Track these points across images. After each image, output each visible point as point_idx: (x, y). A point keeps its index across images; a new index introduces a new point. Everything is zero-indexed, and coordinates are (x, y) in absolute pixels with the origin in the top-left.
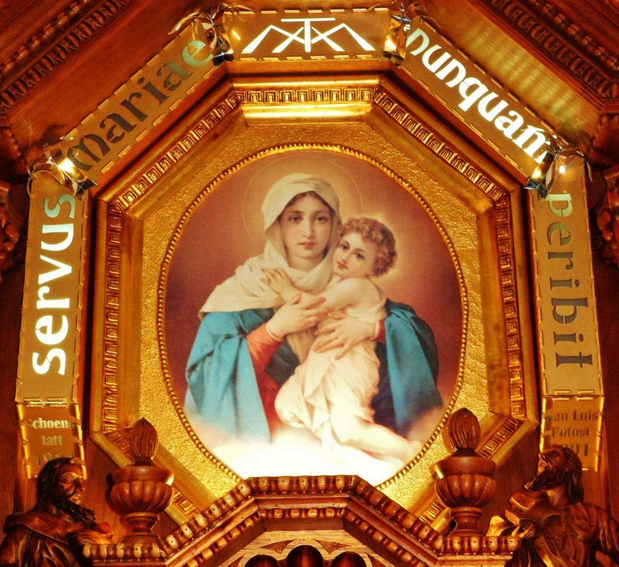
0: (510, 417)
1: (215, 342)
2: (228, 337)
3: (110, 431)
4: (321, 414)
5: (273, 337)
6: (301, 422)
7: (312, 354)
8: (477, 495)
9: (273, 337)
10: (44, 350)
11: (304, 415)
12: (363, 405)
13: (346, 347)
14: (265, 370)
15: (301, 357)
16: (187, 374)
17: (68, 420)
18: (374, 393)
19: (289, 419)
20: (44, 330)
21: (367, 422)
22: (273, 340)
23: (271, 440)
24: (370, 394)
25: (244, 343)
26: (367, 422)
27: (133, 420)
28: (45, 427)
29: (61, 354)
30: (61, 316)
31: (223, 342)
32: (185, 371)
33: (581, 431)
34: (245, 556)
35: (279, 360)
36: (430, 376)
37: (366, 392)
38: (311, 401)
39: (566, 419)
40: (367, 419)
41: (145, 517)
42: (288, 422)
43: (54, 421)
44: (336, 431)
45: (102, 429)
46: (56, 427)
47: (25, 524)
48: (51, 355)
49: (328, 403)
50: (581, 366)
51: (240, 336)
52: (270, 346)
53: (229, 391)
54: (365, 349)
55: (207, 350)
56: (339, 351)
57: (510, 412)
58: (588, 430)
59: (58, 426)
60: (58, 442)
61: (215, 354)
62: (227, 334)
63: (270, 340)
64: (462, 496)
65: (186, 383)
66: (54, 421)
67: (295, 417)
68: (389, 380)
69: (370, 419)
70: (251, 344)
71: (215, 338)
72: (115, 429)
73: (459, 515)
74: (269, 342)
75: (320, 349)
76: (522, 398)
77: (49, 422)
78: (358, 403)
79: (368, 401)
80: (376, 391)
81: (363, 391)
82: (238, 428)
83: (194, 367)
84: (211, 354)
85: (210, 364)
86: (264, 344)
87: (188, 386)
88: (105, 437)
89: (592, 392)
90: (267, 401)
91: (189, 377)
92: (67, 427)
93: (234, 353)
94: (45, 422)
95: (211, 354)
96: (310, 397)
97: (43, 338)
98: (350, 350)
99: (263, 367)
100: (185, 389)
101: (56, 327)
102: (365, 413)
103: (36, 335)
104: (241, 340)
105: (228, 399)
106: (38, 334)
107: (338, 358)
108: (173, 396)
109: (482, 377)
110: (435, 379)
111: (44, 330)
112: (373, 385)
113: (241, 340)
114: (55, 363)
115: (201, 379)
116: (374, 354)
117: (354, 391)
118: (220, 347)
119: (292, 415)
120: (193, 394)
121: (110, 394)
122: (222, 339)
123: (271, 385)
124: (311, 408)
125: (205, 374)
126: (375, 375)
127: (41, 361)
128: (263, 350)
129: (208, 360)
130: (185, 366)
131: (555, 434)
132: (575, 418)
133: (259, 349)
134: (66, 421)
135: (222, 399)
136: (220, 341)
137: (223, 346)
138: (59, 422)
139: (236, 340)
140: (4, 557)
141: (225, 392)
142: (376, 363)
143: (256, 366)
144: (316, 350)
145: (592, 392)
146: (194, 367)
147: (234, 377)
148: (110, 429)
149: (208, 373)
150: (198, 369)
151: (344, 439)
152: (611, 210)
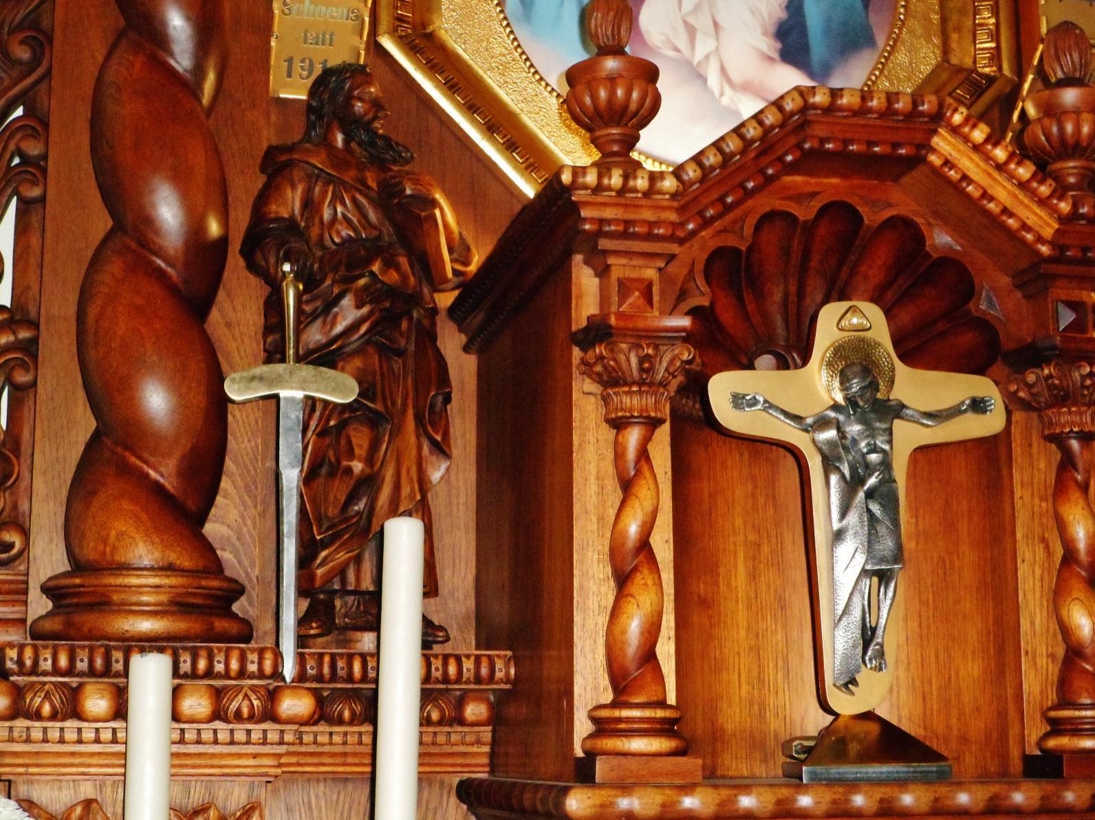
0: (974, 70)
4: (704, 46)
6: (677, 50)
8: (1084, 144)
11: (682, 43)
12: (765, 33)
18: (780, 18)
19: (660, 44)
24: (775, 19)
26: (771, 59)
27: (304, 571)
34: (822, 194)
37: (770, 15)
38: (692, 20)
41: (618, 134)
42: (658, 47)
44: (727, 66)
47: (644, 553)
49: (716, 24)
50: (1091, 5)
57: (975, 62)
64: (1077, 145)
67: (668, 41)
69: (776, 56)
76: (993, 45)
78: (759, 30)
79: (772, 29)
80: (783, 15)
81: (765, 14)
88: (399, 40)
96: (687, 14)
102: (770, 46)
109: (933, 11)
112: (780, 6)
117: (752, 12)
119: (663, 38)
124: (691, 31)
140: (204, 628)
151: (736, 77)
152: (181, 287)
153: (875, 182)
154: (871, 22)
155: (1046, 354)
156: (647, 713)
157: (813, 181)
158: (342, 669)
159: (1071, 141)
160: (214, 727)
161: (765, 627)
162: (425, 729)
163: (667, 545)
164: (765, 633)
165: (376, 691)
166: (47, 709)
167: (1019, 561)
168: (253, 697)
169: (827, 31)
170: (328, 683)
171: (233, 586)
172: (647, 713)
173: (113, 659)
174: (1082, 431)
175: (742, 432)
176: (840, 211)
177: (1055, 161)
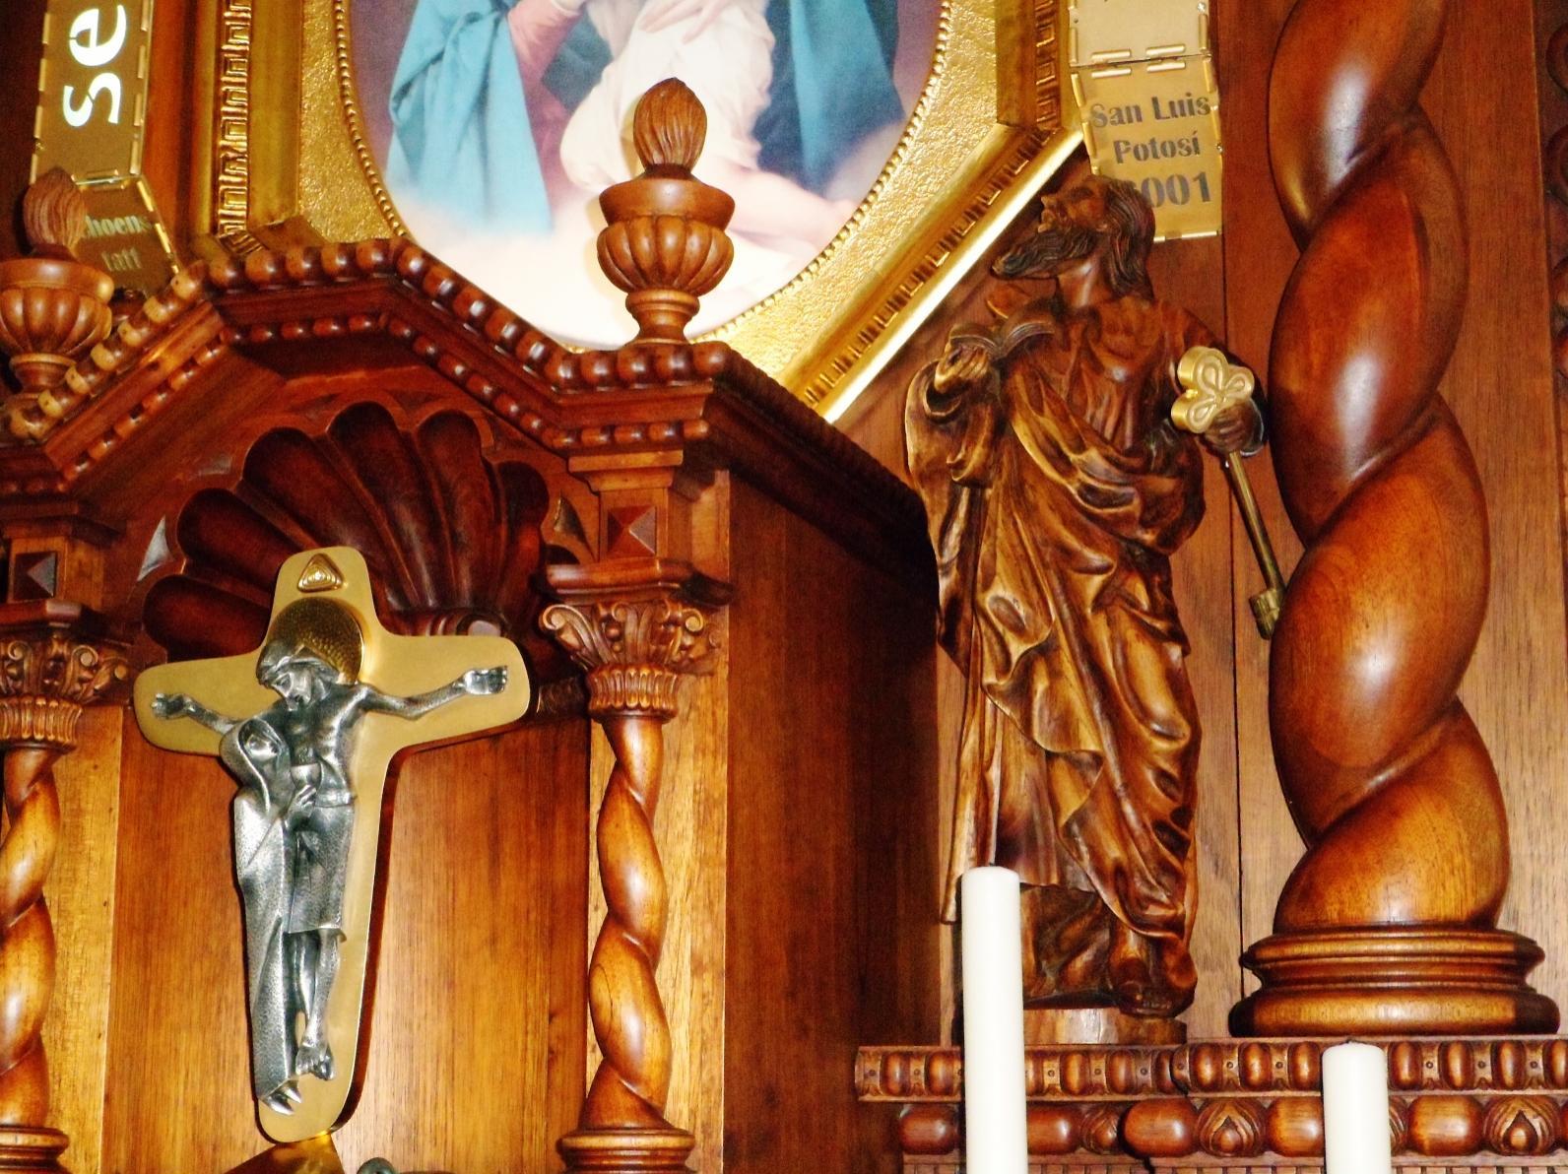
1: (446, 33)
2: (473, 18)
3: (231, 233)
5: (562, 10)
7: (637, 34)
9: (562, 10)
10: (81, 76)
12: (736, 134)
13: (705, 14)
14: (543, 80)
15: (613, 46)
16: (392, 104)
17: (137, 216)
20: (83, 39)
21: (745, 169)
22: (560, 15)
23: (552, 226)
25: (503, 25)
26: (745, 169)
28: (101, 234)
29: (111, 82)
30: (93, 6)
31: (462, 30)
32: (388, 98)
33: (1181, 145)
35: (570, 55)
36: (879, 60)
39: (1140, 119)
40: (746, 165)
42: (587, 184)
43: (112, 219)
45: (215, 228)
46: (120, 231)
48: (95, 87)
51: (496, 14)
52: (556, 27)
53: (473, 131)
54: (746, 14)
55: (431, 53)
56: (691, 24)
58: (1195, 141)
59: (123, 228)
60: (133, 263)
61: (447, 58)
62: (469, 15)
63: (556, 19)
65: (390, 124)
66: (112, 219)
68: (792, 75)
69: (752, 163)
70: (517, 29)
71: (447, 24)
72: (241, 228)
73: (655, 307)
74: (551, 19)
75: (654, 24)
77: (103, 221)
79: (748, 125)
82: (488, 204)
83: (405, 90)
84: (439, 58)
85: (436, 78)
86: (541, 26)
87: (395, 129)
89: (1128, 54)
90: (545, 146)
91: (396, 110)
92: (139, 230)
93: (483, 50)
94: (96, 222)
95: (439, 58)
97: (87, 55)
98: (714, 18)
99: (540, 74)
100: (389, 135)
101: (106, 30)
103: (69, 50)
104: (497, 22)
105: (471, 148)
106: (74, 46)
107: (689, 38)
108: (360, 150)
109: (988, 49)
110: (890, 63)
111: (83, 39)
112: (759, 89)
113: (497, 22)
114: (104, 97)
115: (419, 111)
116: (763, 22)
118: (456, 43)
120: (405, 149)
121: (234, 159)
122: (460, 23)
123: (553, 109)
125: (427, 100)
126: (764, 69)
127: (76, 104)
128: (540, 37)
129: (432, 70)
130: (388, 89)
131: (1124, 156)
132: (1158, 116)
133: (533, 38)
134: (134, 218)
135: (459, 148)
136: (455, 30)
137: (463, 37)
138: (121, 220)
139: (484, 27)
141: (465, 132)
142: (766, 41)
143: (525, 76)
144: (644, 28)
145: (1128, 54)
146: (405, 90)
147: (481, 102)
148: (229, 228)
149: (433, 97)
150: (413, 91)
153: (414, 368)
154: (896, 85)
155: (52, 624)
156: (22, 1140)
157: (328, 380)
158: (1482, 1065)
159: (59, 326)
160: (1549, 1164)
161: (423, 1013)
162: (1402, 1160)
163: (105, 909)
164: (422, 1022)
165: (962, 1105)
166: (1520, 1136)
167: (591, 907)
168: (1529, 1115)
169: (828, 115)
170: (1511, 1089)
171: (1523, 948)
172: (22, 1140)
173: (1528, 1062)
174: (651, 708)
175: (450, 735)
176: (362, 419)
177: (18, 353)
